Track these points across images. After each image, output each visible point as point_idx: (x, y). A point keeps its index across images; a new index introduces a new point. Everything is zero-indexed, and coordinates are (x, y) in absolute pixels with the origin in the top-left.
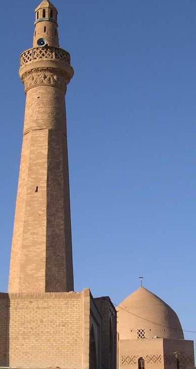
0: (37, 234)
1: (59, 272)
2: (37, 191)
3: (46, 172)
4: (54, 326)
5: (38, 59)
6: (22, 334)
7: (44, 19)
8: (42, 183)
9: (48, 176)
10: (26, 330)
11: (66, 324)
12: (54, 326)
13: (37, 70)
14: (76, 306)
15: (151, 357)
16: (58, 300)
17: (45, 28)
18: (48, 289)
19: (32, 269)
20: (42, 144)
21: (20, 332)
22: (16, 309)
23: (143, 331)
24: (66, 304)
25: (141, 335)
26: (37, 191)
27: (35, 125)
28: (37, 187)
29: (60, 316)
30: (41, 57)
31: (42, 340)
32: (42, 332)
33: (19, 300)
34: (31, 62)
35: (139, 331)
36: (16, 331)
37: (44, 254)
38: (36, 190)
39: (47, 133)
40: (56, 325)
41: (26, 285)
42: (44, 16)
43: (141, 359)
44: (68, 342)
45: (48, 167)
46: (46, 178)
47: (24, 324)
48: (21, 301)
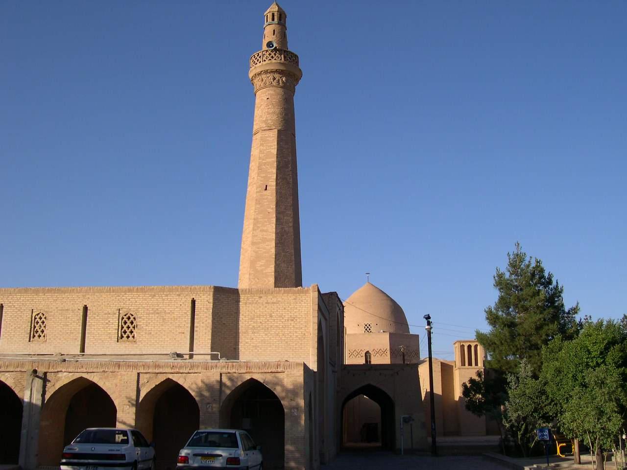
0: (266, 231)
2: (266, 189)
3: (275, 171)
7: (273, 22)
8: (272, 182)
11: (294, 318)
14: (304, 301)
15: (378, 351)
17: (274, 31)
19: (261, 266)
24: (295, 299)
26: (266, 189)
28: (266, 186)
29: (288, 311)
30: (270, 60)
31: (271, 334)
32: (271, 326)
34: (260, 64)
35: (366, 325)
38: (265, 188)
39: (277, 133)
40: (285, 320)
41: (256, 281)
42: (273, 19)
44: (297, 336)
47: (253, 319)
48: (251, 296)
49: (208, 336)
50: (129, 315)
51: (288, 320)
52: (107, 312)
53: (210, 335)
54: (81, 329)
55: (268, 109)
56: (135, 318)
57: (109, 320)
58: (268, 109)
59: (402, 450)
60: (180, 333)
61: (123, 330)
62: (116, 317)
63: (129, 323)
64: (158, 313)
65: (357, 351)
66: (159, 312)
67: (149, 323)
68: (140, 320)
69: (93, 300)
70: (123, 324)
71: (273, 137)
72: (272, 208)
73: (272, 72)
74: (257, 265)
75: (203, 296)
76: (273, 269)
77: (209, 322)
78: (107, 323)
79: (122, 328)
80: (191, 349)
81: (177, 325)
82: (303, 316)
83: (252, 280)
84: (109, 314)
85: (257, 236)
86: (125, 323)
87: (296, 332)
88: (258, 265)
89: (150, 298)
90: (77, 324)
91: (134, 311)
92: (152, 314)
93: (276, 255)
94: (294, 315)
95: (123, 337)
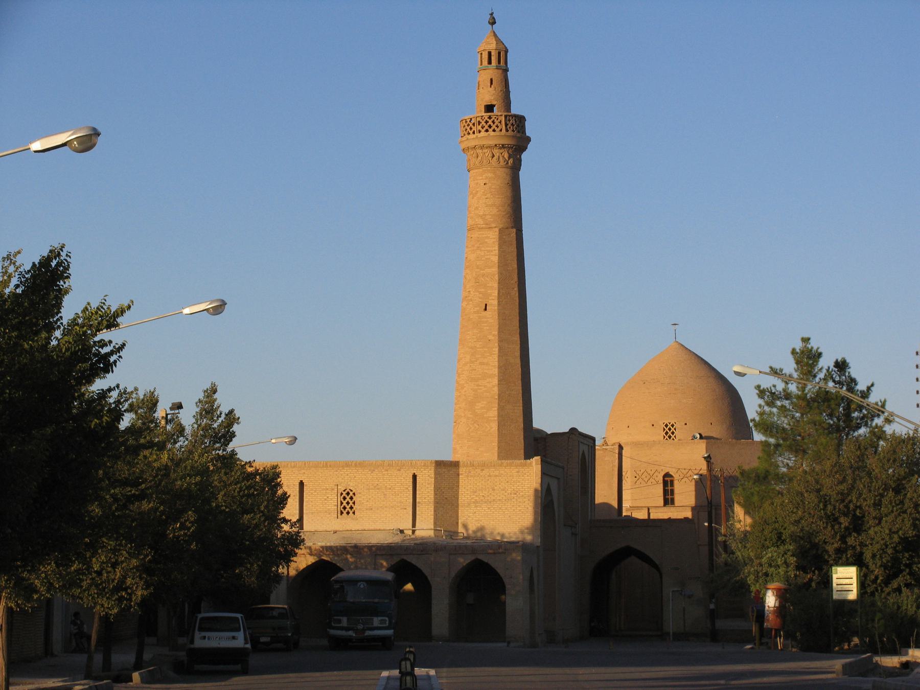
0: (487, 364)
1: (514, 410)
3: (496, 285)
4: (506, 494)
5: (483, 134)
6: (474, 502)
8: (493, 300)
9: (499, 291)
10: (477, 498)
12: (506, 494)
13: (482, 147)
16: (509, 468)
17: (491, 80)
18: (500, 457)
20: (491, 249)
21: (473, 500)
22: (468, 476)
23: (673, 426)
24: (518, 472)
25: (670, 433)
27: (482, 222)
28: (486, 305)
29: (511, 484)
32: (494, 500)
33: (470, 468)
34: (474, 136)
35: (666, 426)
36: (468, 499)
37: (496, 389)
38: (484, 308)
39: (497, 233)
41: (475, 427)
42: (490, 62)
43: (667, 475)
44: (520, 510)
45: (499, 280)
46: (497, 293)
47: (475, 492)
48: (473, 468)
49: (431, 512)
50: (348, 490)
51: (511, 494)
52: (325, 488)
53: (433, 511)
54: (298, 505)
55: (486, 198)
56: (354, 494)
57: (328, 495)
58: (486, 198)
59: (671, 634)
60: (402, 508)
61: (342, 506)
62: (334, 493)
63: (348, 499)
64: (378, 489)
65: (649, 472)
66: (379, 487)
67: (370, 498)
68: (360, 495)
69: (309, 475)
70: (342, 500)
71: (494, 238)
72: (494, 335)
73: (489, 147)
74: (476, 407)
75: (424, 470)
76: (496, 413)
77: (431, 498)
78: (325, 499)
79: (342, 503)
80: (414, 525)
81: (399, 501)
82: (526, 490)
83: (471, 426)
84: (327, 489)
85: (475, 370)
86: (344, 498)
87: (519, 506)
88: (479, 407)
89: (370, 472)
90: (293, 501)
91: (353, 486)
92: (372, 489)
93: (499, 395)
94: (517, 488)
95: (343, 513)
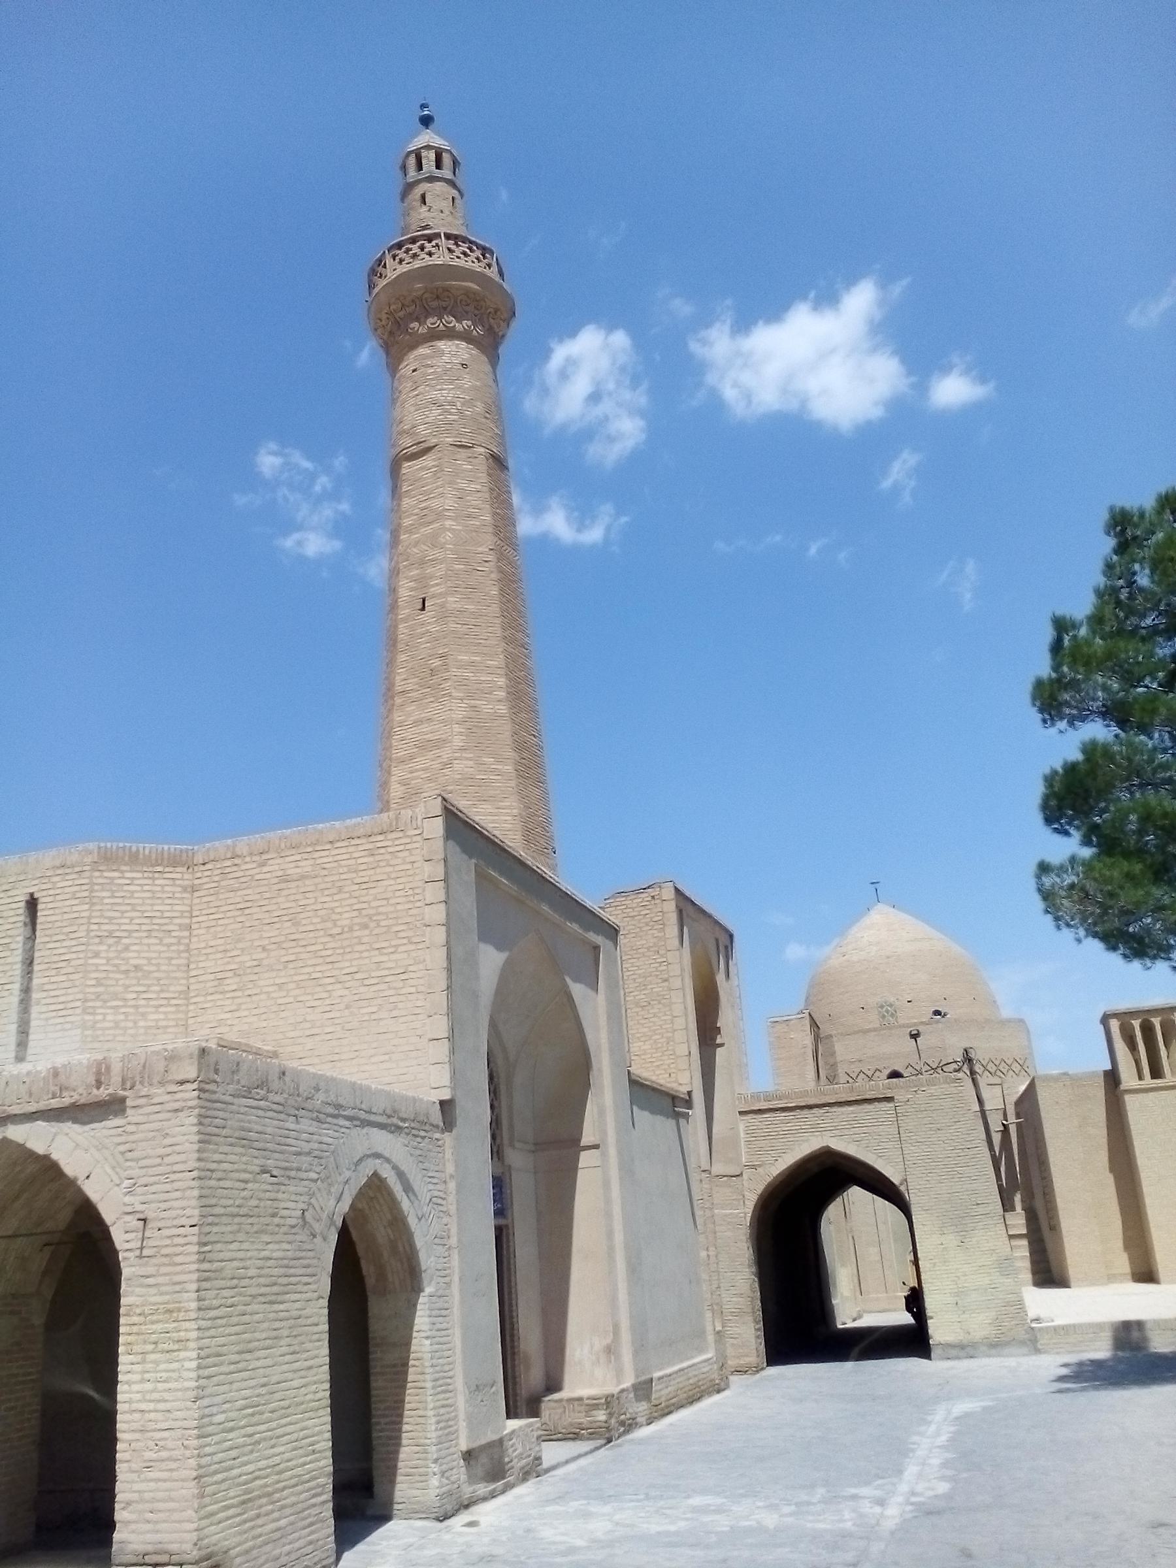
2: (423, 608)
8: (437, 585)
11: (370, 917)
40: (343, 927)
